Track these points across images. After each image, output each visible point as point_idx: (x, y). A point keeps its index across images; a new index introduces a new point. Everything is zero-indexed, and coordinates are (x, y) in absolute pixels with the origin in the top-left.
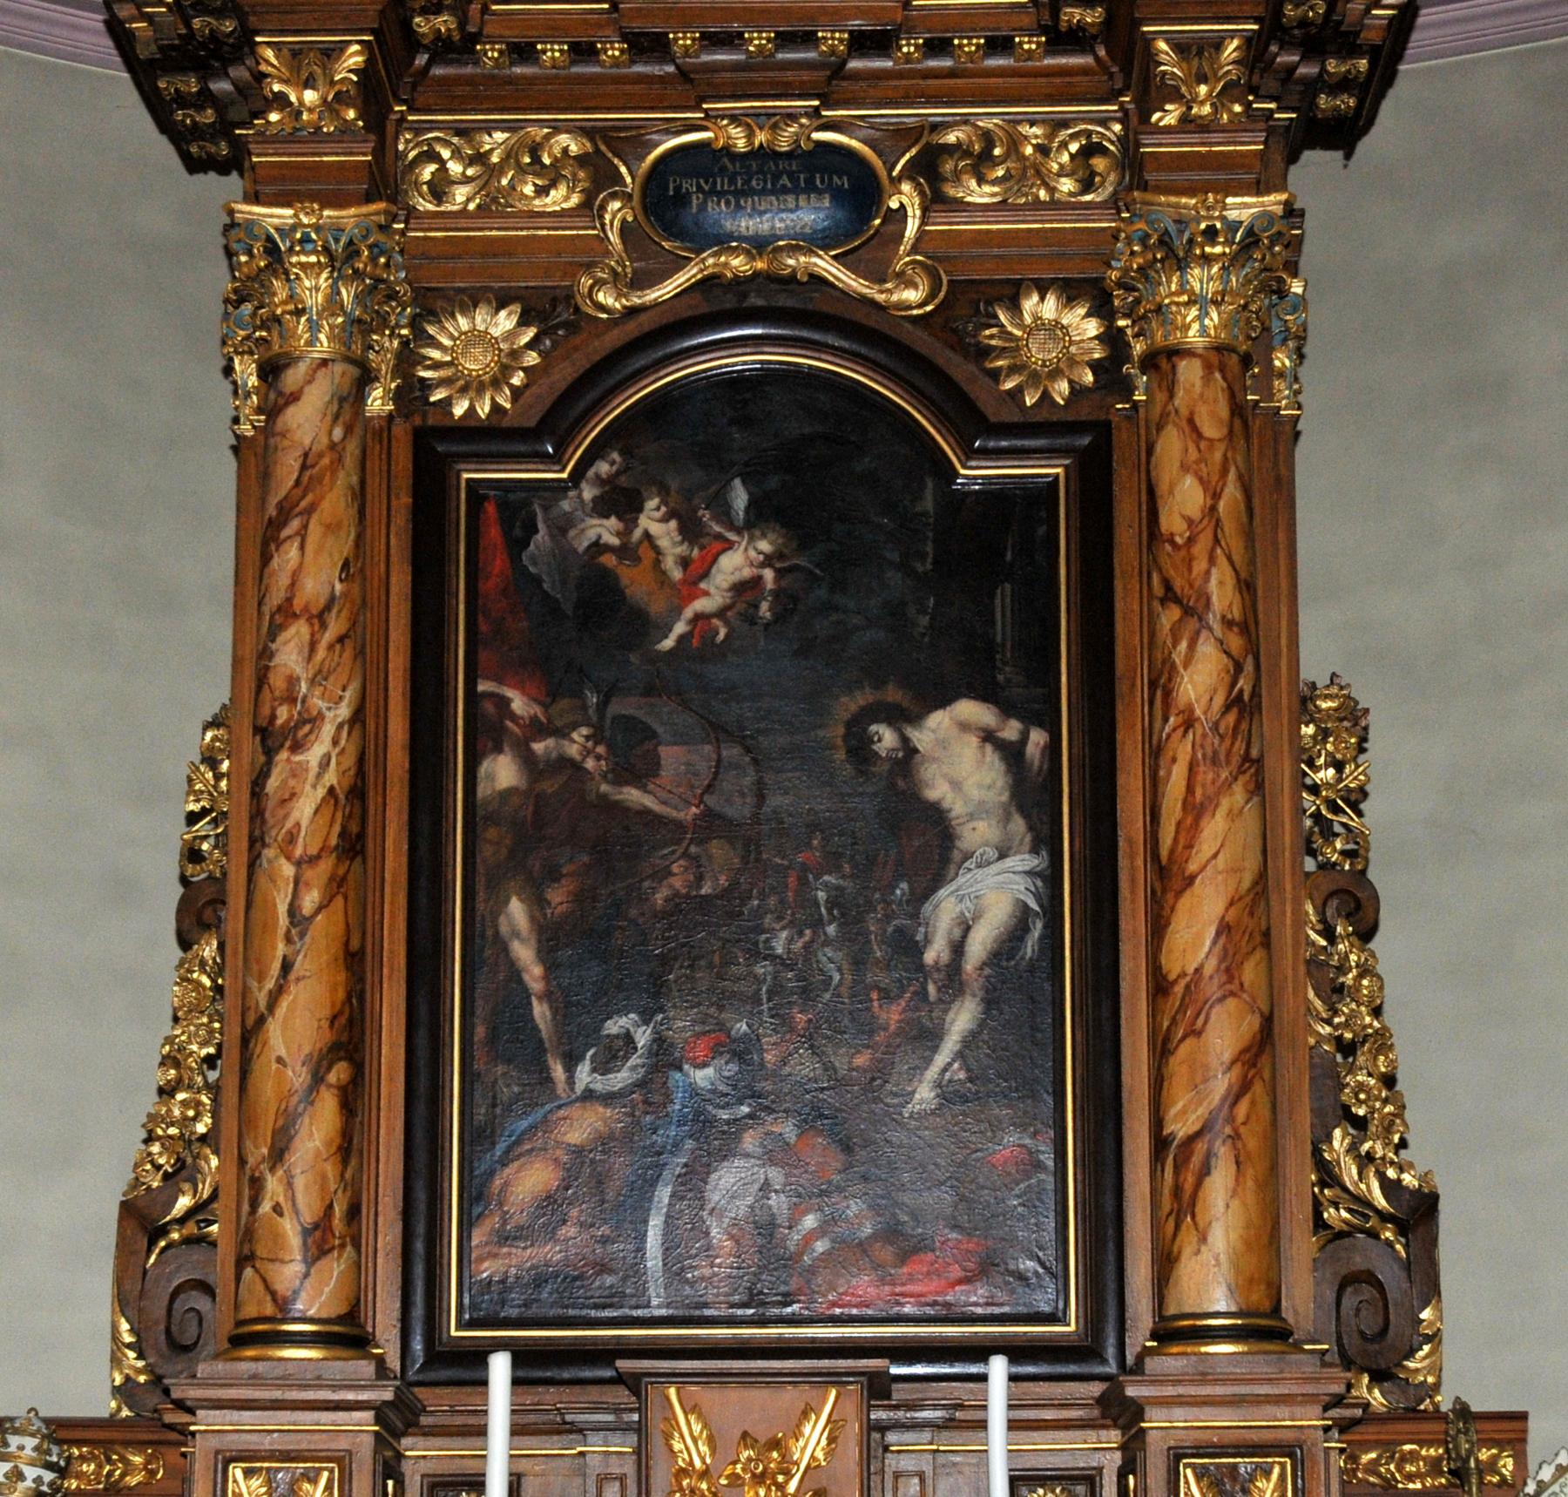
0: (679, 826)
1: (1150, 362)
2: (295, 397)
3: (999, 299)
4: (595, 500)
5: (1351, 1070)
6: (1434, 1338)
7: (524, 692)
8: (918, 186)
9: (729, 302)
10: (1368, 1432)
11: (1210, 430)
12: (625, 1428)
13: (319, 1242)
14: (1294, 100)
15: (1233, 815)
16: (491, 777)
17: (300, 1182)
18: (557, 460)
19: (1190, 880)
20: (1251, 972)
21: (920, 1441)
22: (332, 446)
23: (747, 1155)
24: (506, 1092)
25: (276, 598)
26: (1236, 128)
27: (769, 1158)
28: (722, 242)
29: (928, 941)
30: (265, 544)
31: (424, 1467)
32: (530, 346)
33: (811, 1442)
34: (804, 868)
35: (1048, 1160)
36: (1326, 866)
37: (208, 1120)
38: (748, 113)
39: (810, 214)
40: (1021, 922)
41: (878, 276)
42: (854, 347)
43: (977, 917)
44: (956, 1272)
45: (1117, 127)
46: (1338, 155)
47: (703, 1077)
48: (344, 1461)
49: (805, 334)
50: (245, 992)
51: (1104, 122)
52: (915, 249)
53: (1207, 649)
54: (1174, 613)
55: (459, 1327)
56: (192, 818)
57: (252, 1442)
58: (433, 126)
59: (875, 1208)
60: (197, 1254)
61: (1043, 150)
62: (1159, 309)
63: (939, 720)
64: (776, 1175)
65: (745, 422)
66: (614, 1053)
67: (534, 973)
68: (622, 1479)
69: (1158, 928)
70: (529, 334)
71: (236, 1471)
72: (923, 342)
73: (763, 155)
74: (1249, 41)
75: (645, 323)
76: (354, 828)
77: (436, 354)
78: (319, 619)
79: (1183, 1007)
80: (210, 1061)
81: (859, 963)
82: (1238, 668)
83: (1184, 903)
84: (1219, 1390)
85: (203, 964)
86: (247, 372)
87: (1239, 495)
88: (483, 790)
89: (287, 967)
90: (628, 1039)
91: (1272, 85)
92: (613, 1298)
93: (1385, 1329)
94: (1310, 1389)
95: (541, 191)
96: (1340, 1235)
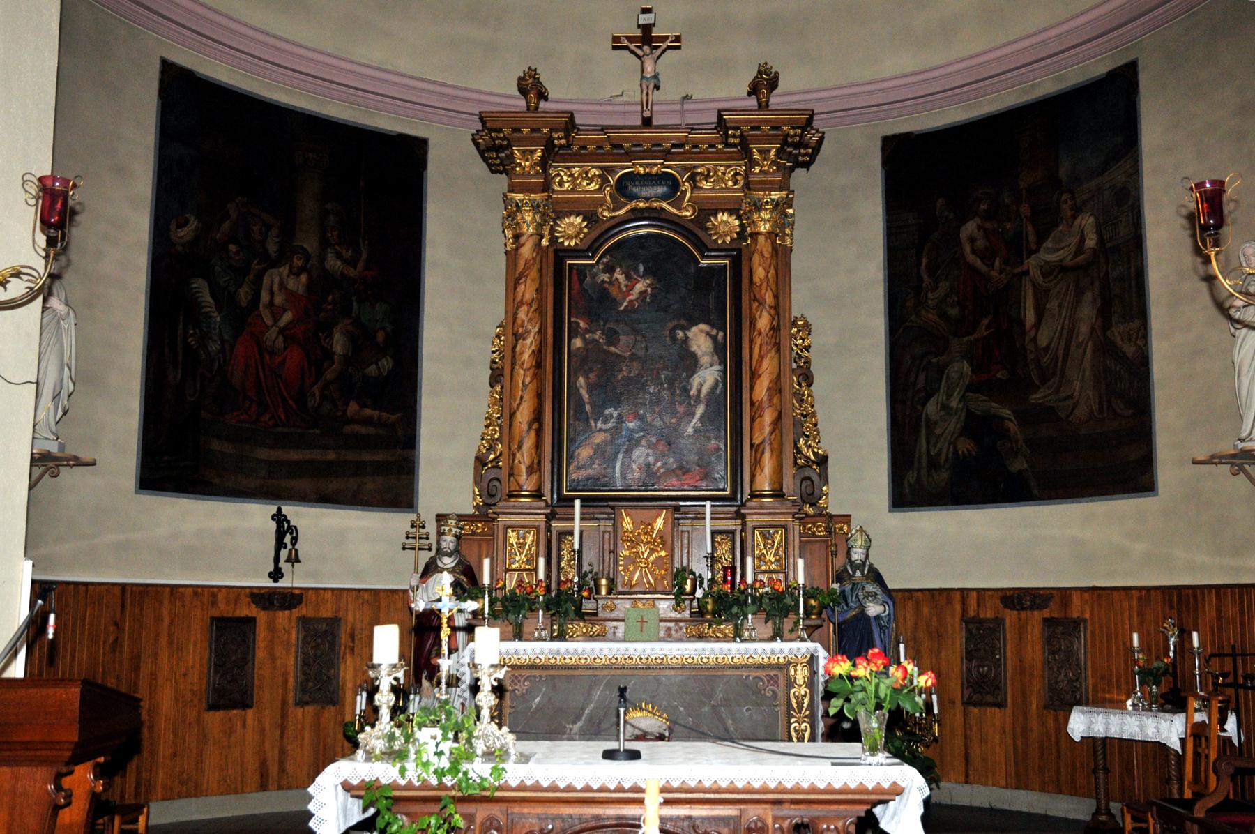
1: (751, 235)
2: (523, 245)
3: (711, 215)
4: (603, 269)
5: (805, 422)
6: (826, 495)
7: (584, 321)
8: (690, 184)
9: (639, 215)
10: (808, 519)
11: (767, 255)
13: (530, 470)
14: (792, 160)
15: (772, 358)
16: (575, 344)
17: (525, 455)
18: (592, 258)
19: (760, 376)
20: (775, 400)
21: (688, 523)
22: (533, 258)
23: (643, 446)
24: (578, 429)
25: (519, 299)
26: (774, 173)
27: (649, 447)
28: (636, 198)
29: (691, 389)
30: (515, 284)
31: (557, 529)
32: (585, 227)
33: (659, 523)
34: (659, 369)
35: (723, 448)
36: (799, 367)
37: (498, 434)
38: (644, 163)
39: (661, 190)
40: (716, 383)
41: (679, 209)
42: (670, 227)
43: (705, 382)
45: (744, 168)
46: (805, 170)
47: (631, 425)
48: (537, 528)
49: (659, 224)
50: (511, 404)
51: (740, 166)
52: (689, 201)
53: (765, 314)
54: (757, 304)
55: (567, 491)
56: (493, 352)
57: (514, 523)
58: (559, 166)
59: (677, 461)
60: (496, 470)
61: (724, 174)
62: (753, 222)
63: (694, 329)
64: (650, 452)
65: (643, 248)
66: (607, 419)
67: (586, 396)
68: (609, 532)
69: (752, 388)
70: (585, 223)
71: (509, 531)
72: (691, 226)
73: (647, 175)
74: (778, 149)
75: (616, 220)
76: (539, 360)
77: (560, 229)
78: (530, 305)
79: (757, 410)
80: (498, 418)
81: (673, 394)
82: (773, 319)
83: (758, 382)
84: (765, 511)
85: (497, 392)
86: (509, 233)
87: (774, 272)
88: (572, 348)
89: (522, 398)
90: (611, 415)
93: (813, 492)
94: (789, 511)
95: (588, 184)
96: (802, 467)
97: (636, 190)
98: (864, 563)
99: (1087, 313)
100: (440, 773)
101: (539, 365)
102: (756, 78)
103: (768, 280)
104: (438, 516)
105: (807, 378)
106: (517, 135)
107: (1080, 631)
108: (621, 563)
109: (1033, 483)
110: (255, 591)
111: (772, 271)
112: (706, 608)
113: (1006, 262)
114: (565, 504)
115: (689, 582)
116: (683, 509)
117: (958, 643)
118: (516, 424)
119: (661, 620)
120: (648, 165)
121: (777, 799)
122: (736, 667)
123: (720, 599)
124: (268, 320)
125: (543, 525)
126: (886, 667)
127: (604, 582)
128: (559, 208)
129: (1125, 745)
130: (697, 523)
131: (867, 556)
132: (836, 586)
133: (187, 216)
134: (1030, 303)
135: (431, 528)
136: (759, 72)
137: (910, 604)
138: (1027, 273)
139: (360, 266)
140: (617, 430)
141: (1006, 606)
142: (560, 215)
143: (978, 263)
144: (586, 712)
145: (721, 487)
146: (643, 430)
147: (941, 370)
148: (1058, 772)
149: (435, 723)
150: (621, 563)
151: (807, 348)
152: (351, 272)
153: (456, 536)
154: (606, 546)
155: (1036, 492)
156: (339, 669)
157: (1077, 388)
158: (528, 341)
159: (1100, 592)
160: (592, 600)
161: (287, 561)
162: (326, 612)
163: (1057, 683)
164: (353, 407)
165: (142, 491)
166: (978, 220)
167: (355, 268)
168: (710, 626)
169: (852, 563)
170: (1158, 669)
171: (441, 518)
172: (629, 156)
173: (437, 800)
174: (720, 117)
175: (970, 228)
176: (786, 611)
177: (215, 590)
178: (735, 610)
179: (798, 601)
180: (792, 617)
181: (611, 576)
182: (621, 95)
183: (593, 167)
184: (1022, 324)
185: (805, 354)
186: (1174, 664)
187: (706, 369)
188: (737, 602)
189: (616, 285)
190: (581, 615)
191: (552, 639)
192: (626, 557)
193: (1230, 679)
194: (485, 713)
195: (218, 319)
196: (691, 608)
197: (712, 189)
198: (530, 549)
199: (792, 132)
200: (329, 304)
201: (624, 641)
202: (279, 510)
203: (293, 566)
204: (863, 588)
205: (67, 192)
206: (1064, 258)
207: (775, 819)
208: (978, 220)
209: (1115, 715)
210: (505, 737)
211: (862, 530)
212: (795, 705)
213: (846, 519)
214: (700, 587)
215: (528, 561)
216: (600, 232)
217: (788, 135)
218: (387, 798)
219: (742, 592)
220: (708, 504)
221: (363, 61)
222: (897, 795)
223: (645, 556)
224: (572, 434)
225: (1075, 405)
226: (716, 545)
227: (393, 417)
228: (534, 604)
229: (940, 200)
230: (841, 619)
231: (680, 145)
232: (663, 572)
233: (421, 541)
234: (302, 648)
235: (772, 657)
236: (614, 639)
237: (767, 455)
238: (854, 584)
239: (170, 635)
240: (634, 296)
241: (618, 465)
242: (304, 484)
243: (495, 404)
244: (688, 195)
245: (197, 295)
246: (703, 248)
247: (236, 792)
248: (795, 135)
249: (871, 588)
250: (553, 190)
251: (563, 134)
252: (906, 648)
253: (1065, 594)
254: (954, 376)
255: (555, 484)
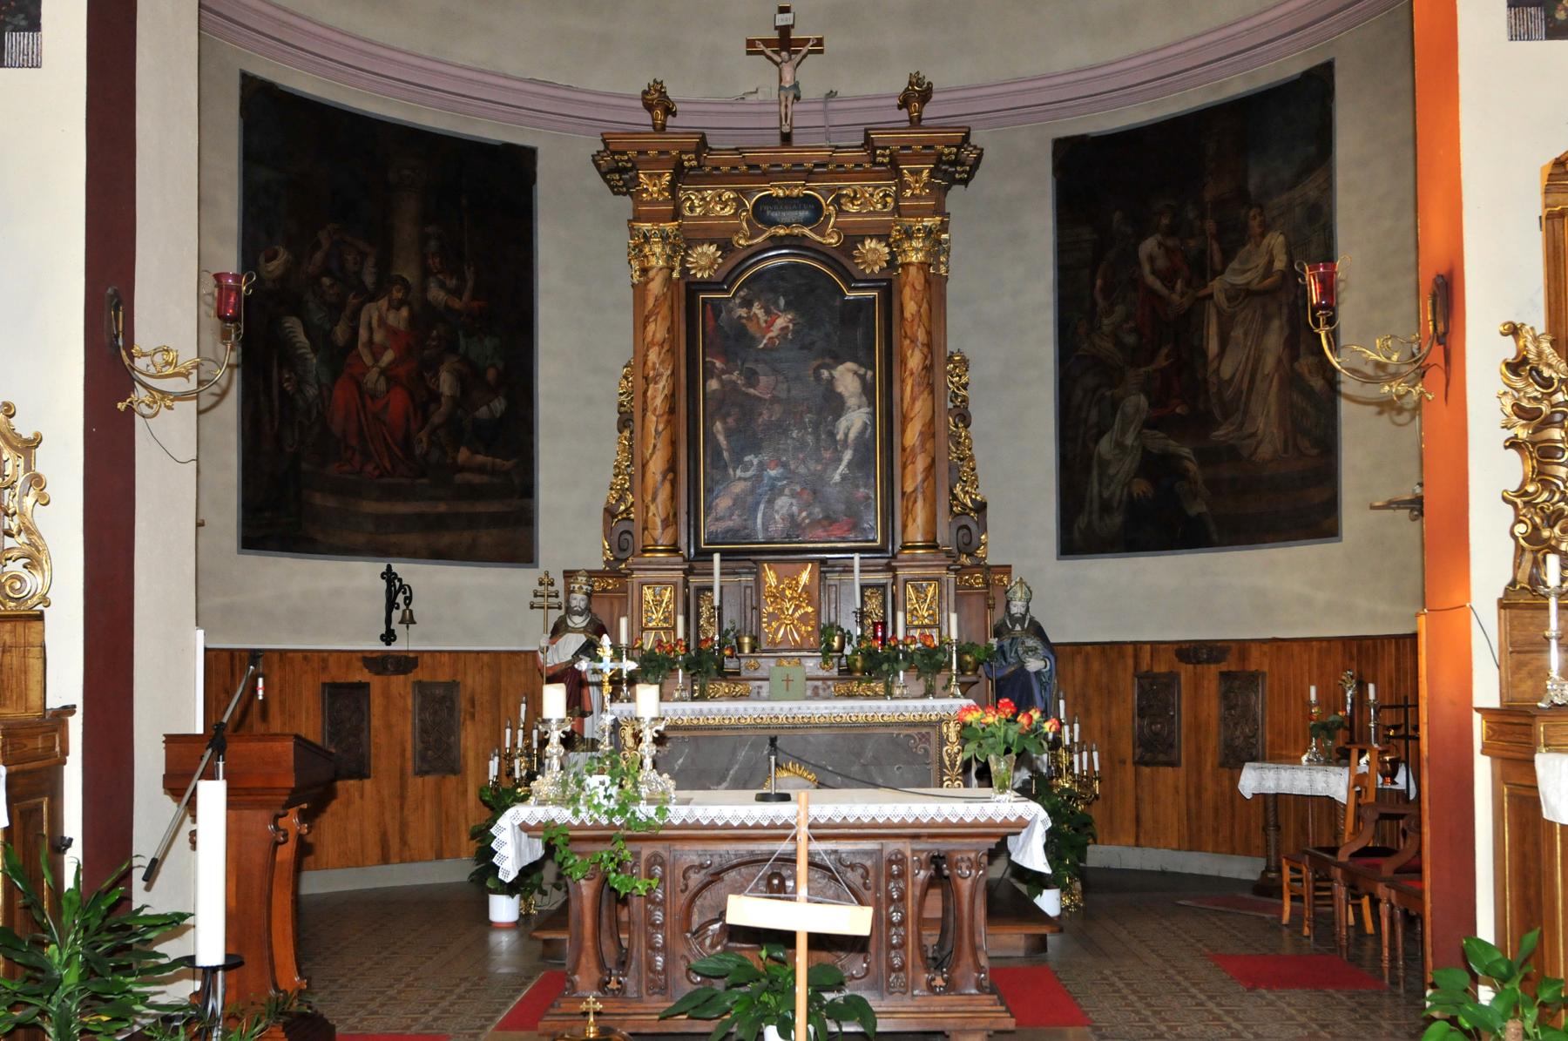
0: (765, 400)
2: (653, 280)
5: (962, 466)
6: (985, 544)
10: (964, 571)
11: (919, 287)
12: (753, 573)
13: (666, 523)
15: (924, 401)
17: (660, 508)
18: (727, 291)
21: (836, 576)
22: (664, 294)
33: (805, 577)
41: (823, 236)
43: (852, 425)
44: (846, 528)
46: (963, 187)
47: (773, 473)
48: (675, 584)
50: (642, 452)
51: (890, 186)
56: (621, 394)
58: (689, 189)
60: (627, 523)
61: (872, 195)
63: (841, 368)
64: (794, 501)
65: (783, 279)
68: (751, 587)
69: (903, 431)
70: (720, 253)
71: (645, 588)
72: (836, 255)
73: (787, 198)
74: (931, 170)
78: (662, 345)
80: (628, 466)
81: (818, 439)
82: (926, 358)
86: (636, 265)
88: (708, 390)
89: (655, 446)
90: (752, 464)
91: (940, 175)
92: (748, 536)
95: (722, 209)
96: (958, 515)
97: (775, 215)
98: (1024, 616)
99: (1274, 341)
100: (610, 813)
101: (672, 411)
102: (907, 89)
103: (921, 316)
104: (565, 572)
105: (964, 418)
106: (643, 157)
107: (1258, 685)
108: (765, 620)
109: (1212, 528)
110: (368, 655)
111: (925, 306)
112: (855, 665)
113: (1188, 283)
114: (703, 558)
115: (836, 638)
116: (830, 562)
117: (1130, 698)
118: (649, 475)
119: (808, 679)
120: (788, 187)
121: (914, 832)
122: (887, 725)
123: (870, 655)
124: (368, 360)
125: (680, 581)
126: (1016, 715)
127: (746, 640)
128: (690, 235)
129: (1302, 800)
130: (844, 577)
131: (1027, 609)
132: (994, 641)
133: (277, 247)
134: (1213, 330)
135: (560, 584)
136: (910, 83)
137: (1079, 659)
138: (1211, 296)
139: (466, 297)
140: (758, 478)
141: (1181, 660)
142: (691, 244)
143: (1158, 285)
144: (731, 772)
145: (871, 538)
146: (786, 478)
147: (1115, 405)
148: (1232, 833)
149: (601, 772)
150: (765, 620)
151: (965, 386)
152: (457, 304)
153: (586, 594)
154: (748, 602)
155: (1215, 537)
156: (459, 735)
157: (1261, 425)
158: (660, 385)
159: (1280, 643)
160: (735, 659)
161: (401, 622)
162: (444, 676)
163: (1232, 740)
164: (463, 455)
165: (244, 550)
166: (1159, 236)
167: (461, 299)
168: (859, 684)
169: (1011, 616)
170: (1333, 723)
171: (569, 575)
172: (767, 176)
173: (607, 839)
174: (867, 136)
175: (1149, 246)
176: (938, 667)
177: (326, 654)
178: (885, 667)
179: (951, 657)
180: (944, 673)
181: (754, 633)
182: (756, 92)
183: (727, 189)
184: (1204, 354)
185: (963, 392)
186: (1351, 718)
187: (854, 411)
188: (887, 659)
189: (755, 321)
190: (723, 675)
191: (693, 699)
192: (769, 614)
193: (1402, 732)
194: (648, 762)
195: (315, 361)
196: (839, 666)
197: (859, 213)
198: (667, 607)
199: (946, 151)
200: (434, 340)
201: (768, 699)
202: (389, 567)
203: (408, 627)
204: (1023, 643)
205: (241, 287)
206: (1250, 281)
207: (914, 852)
208: (1159, 236)
209: (1285, 770)
210: (667, 782)
211: (1021, 582)
212: (948, 763)
213: (1006, 570)
214: (849, 643)
215: (666, 620)
216: (735, 262)
217: (942, 154)
218: (564, 835)
219: (894, 648)
220: (857, 556)
221: (461, 62)
222: (1024, 827)
223: (790, 612)
224: (709, 483)
225: (1259, 443)
226: (866, 599)
227: (509, 464)
228: (675, 663)
229: (1118, 213)
230: (1000, 675)
231: (824, 165)
232: (810, 629)
233: (550, 599)
234: (419, 714)
235: (924, 714)
236: (759, 698)
237: (920, 504)
238: (1013, 639)
239: (282, 703)
240: (775, 332)
241: (760, 516)
242: (414, 540)
243: (623, 451)
244: (832, 220)
245: (291, 335)
246: (850, 278)
247: (358, 866)
248: (950, 154)
249: (1030, 643)
250: (683, 216)
251: (693, 156)
252: (1066, 705)
253: (1243, 646)
254: (1130, 409)
255: (692, 537)
